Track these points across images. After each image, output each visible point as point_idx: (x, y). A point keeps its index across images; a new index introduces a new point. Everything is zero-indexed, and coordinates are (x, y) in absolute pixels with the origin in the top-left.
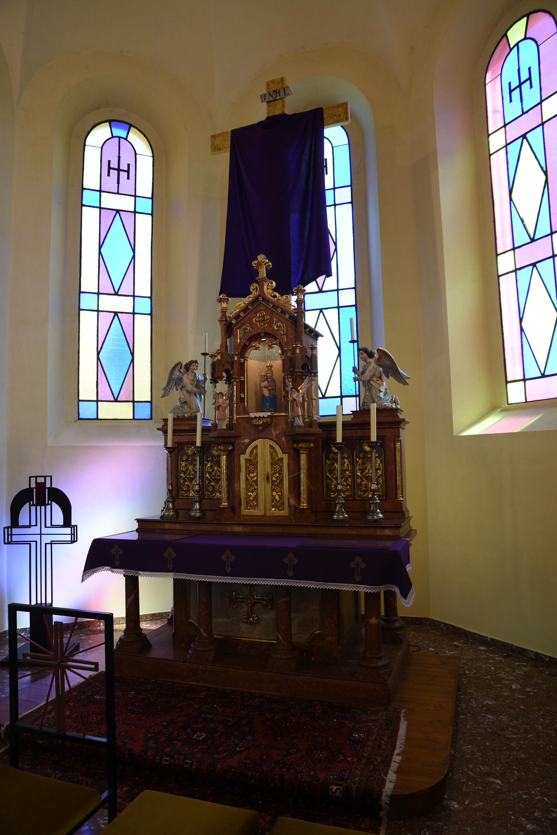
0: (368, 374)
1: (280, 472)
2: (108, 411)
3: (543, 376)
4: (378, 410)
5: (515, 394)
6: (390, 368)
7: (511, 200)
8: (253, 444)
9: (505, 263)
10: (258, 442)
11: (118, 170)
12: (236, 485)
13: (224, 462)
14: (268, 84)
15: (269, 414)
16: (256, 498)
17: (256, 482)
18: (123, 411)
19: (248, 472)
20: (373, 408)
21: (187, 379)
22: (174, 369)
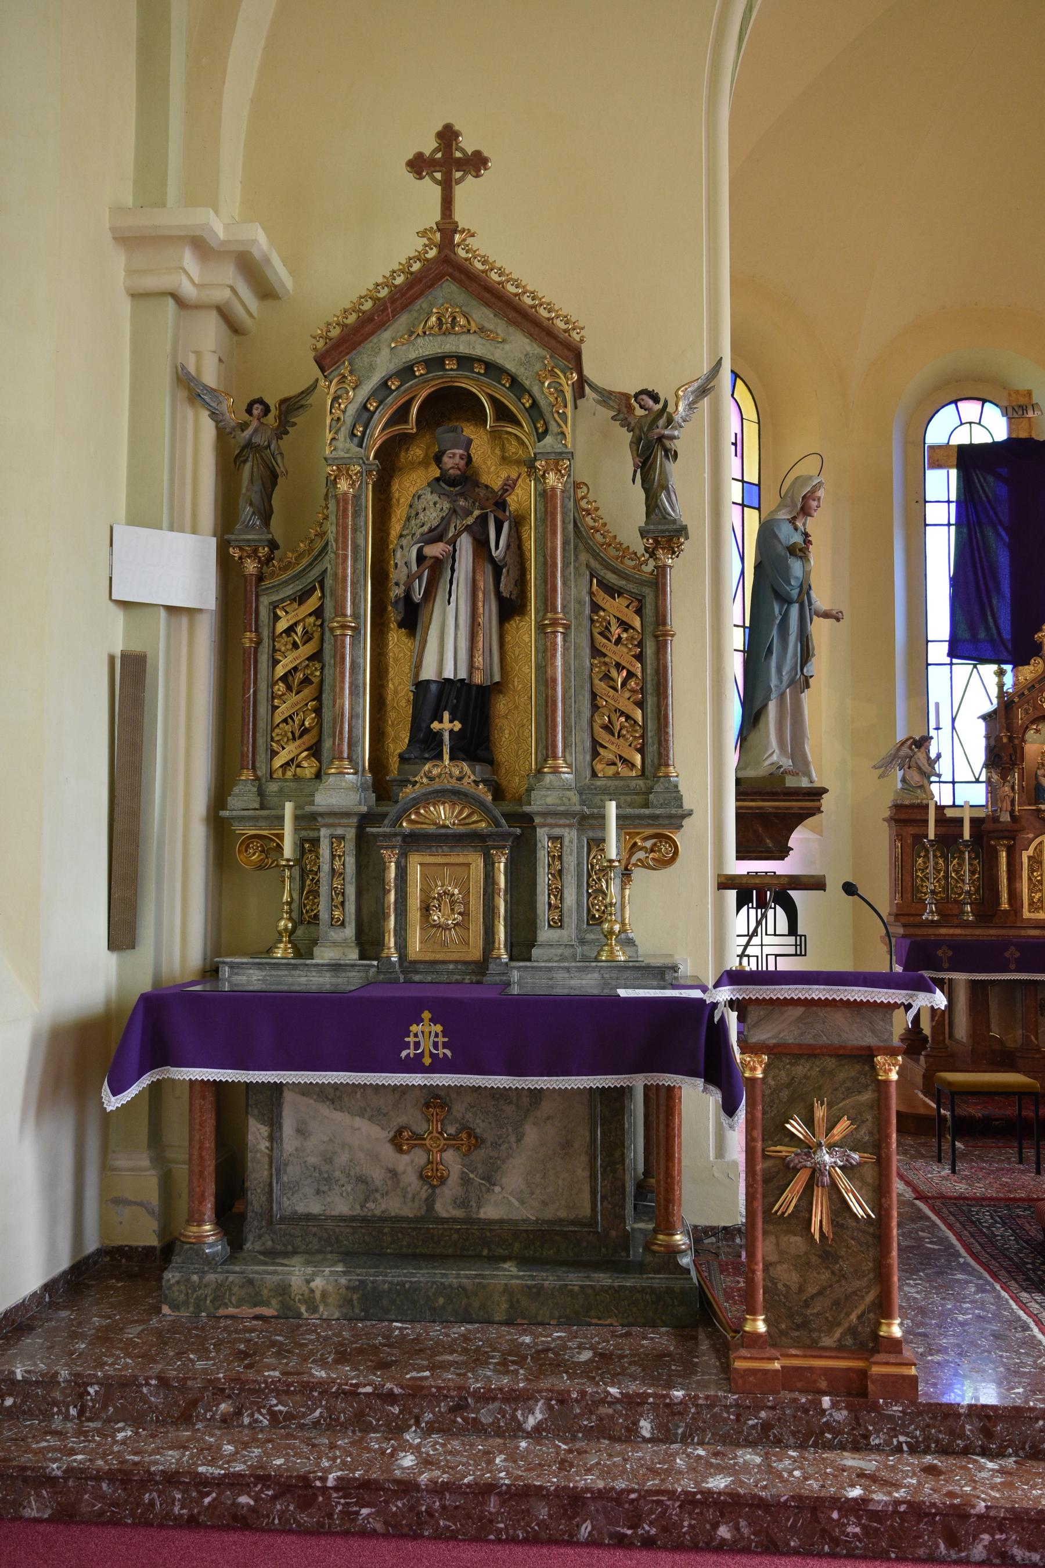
7: (953, 728)
12: (1018, 885)
13: (304, 979)
17: (1041, 882)
19: (1031, 870)
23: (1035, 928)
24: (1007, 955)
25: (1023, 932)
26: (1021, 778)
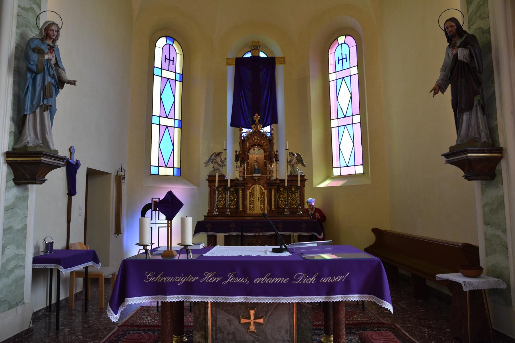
0: (293, 162)
1: (264, 197)
2: (163, 171)
3: (347, 166)
4: (219, 176)
5: (336, 172)
6: (300, 160)
8: (252, 187)
9: (334, 123)
10: (255, 186)
11: (168, 59)
14: (252, 42)
15: (260, 175)
16: (253, 207)
17: (253, 201)
18: (169, 172)
19: (250, 197)
20: (217, 175)
21: (218, 159)
22: (212, 155)
23: (249, 217)
24: (207, 226)
25: (245, 218)
26: (248, 165)
